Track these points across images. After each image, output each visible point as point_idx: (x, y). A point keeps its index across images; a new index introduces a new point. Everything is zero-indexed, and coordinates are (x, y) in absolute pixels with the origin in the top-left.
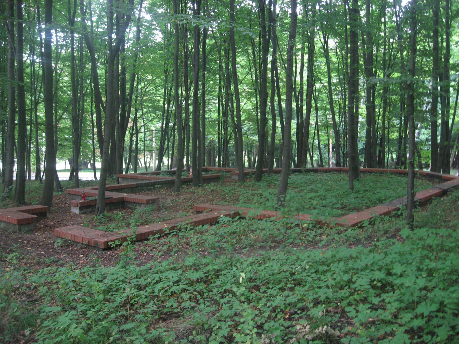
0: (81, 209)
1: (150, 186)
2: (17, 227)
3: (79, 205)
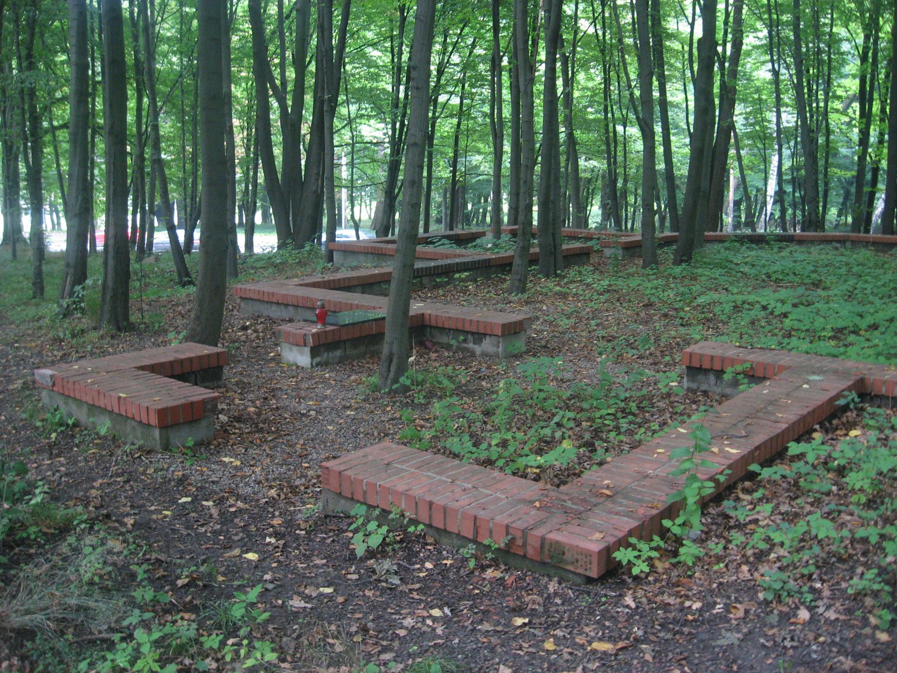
0: (315, 352)
1: (439, 275)
2: (157, 433)
3: (310, 341)
